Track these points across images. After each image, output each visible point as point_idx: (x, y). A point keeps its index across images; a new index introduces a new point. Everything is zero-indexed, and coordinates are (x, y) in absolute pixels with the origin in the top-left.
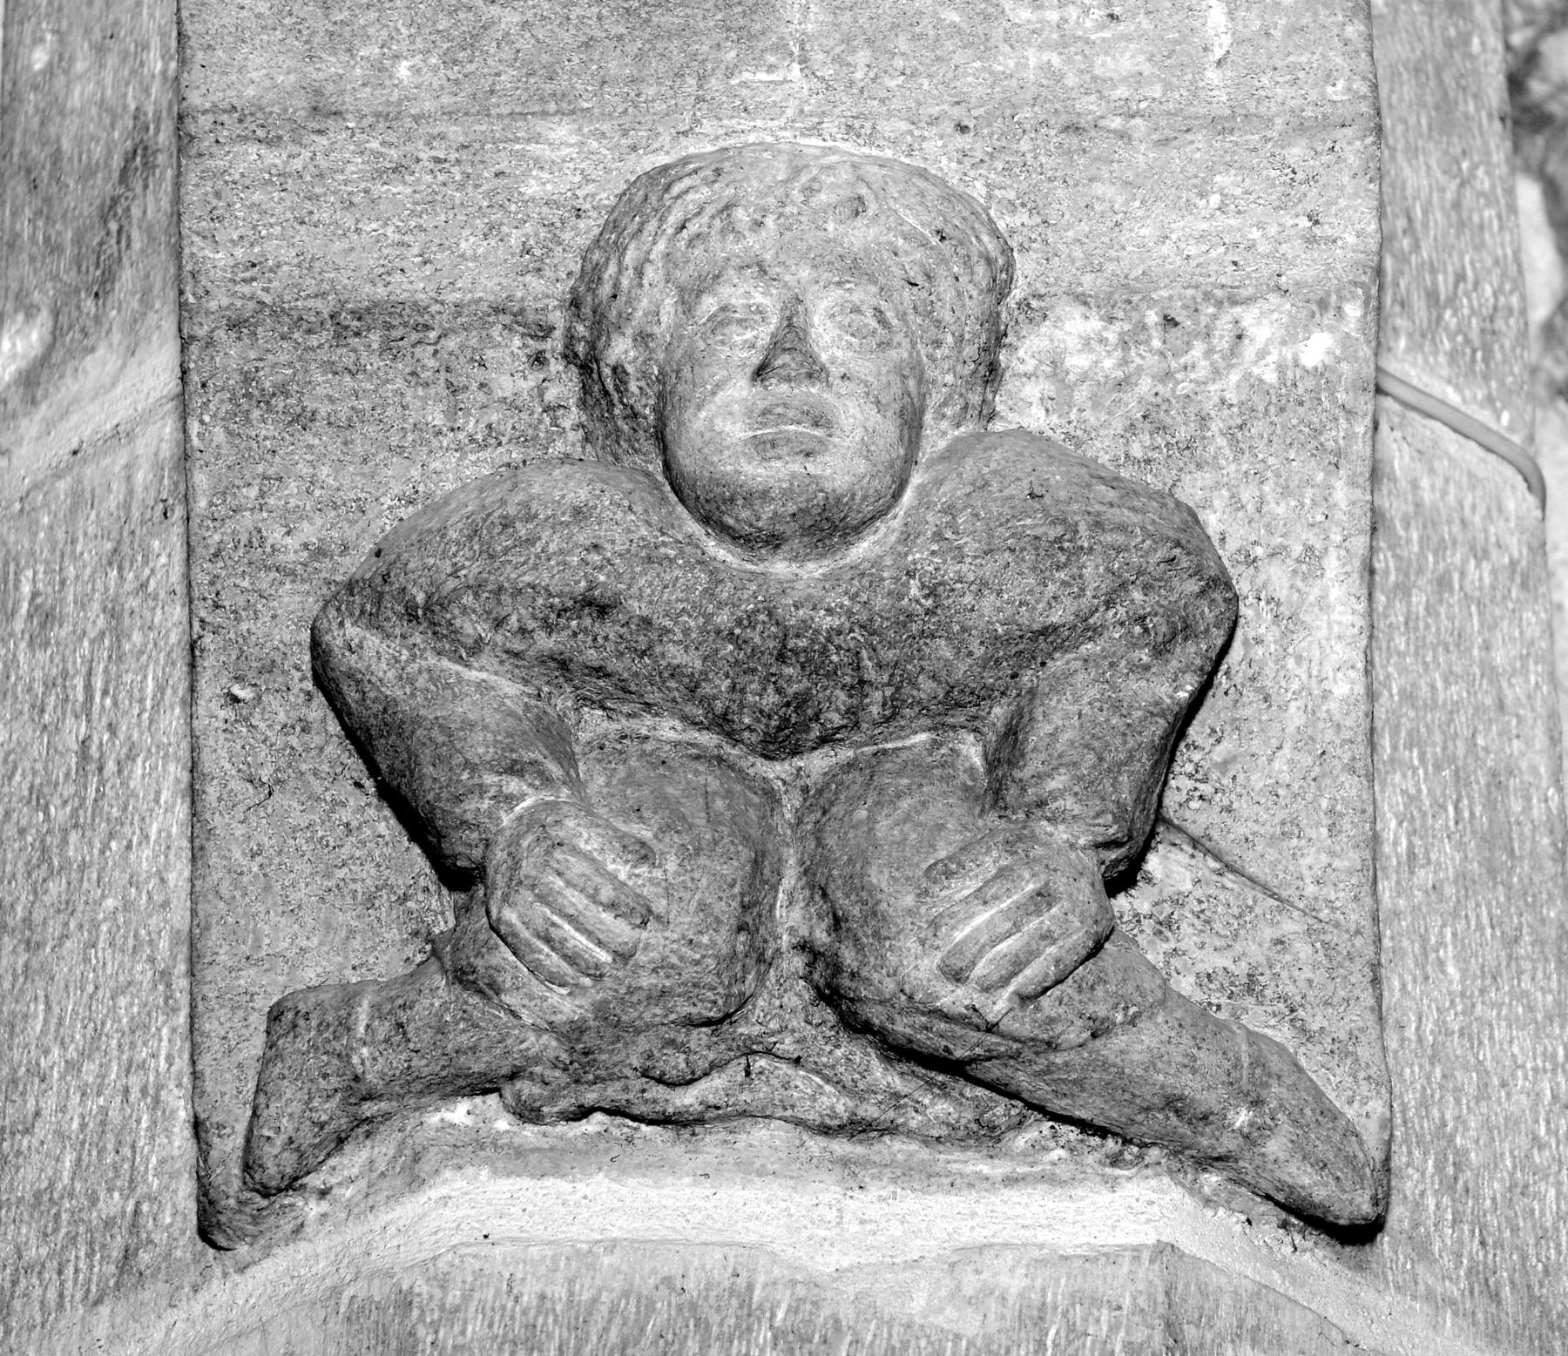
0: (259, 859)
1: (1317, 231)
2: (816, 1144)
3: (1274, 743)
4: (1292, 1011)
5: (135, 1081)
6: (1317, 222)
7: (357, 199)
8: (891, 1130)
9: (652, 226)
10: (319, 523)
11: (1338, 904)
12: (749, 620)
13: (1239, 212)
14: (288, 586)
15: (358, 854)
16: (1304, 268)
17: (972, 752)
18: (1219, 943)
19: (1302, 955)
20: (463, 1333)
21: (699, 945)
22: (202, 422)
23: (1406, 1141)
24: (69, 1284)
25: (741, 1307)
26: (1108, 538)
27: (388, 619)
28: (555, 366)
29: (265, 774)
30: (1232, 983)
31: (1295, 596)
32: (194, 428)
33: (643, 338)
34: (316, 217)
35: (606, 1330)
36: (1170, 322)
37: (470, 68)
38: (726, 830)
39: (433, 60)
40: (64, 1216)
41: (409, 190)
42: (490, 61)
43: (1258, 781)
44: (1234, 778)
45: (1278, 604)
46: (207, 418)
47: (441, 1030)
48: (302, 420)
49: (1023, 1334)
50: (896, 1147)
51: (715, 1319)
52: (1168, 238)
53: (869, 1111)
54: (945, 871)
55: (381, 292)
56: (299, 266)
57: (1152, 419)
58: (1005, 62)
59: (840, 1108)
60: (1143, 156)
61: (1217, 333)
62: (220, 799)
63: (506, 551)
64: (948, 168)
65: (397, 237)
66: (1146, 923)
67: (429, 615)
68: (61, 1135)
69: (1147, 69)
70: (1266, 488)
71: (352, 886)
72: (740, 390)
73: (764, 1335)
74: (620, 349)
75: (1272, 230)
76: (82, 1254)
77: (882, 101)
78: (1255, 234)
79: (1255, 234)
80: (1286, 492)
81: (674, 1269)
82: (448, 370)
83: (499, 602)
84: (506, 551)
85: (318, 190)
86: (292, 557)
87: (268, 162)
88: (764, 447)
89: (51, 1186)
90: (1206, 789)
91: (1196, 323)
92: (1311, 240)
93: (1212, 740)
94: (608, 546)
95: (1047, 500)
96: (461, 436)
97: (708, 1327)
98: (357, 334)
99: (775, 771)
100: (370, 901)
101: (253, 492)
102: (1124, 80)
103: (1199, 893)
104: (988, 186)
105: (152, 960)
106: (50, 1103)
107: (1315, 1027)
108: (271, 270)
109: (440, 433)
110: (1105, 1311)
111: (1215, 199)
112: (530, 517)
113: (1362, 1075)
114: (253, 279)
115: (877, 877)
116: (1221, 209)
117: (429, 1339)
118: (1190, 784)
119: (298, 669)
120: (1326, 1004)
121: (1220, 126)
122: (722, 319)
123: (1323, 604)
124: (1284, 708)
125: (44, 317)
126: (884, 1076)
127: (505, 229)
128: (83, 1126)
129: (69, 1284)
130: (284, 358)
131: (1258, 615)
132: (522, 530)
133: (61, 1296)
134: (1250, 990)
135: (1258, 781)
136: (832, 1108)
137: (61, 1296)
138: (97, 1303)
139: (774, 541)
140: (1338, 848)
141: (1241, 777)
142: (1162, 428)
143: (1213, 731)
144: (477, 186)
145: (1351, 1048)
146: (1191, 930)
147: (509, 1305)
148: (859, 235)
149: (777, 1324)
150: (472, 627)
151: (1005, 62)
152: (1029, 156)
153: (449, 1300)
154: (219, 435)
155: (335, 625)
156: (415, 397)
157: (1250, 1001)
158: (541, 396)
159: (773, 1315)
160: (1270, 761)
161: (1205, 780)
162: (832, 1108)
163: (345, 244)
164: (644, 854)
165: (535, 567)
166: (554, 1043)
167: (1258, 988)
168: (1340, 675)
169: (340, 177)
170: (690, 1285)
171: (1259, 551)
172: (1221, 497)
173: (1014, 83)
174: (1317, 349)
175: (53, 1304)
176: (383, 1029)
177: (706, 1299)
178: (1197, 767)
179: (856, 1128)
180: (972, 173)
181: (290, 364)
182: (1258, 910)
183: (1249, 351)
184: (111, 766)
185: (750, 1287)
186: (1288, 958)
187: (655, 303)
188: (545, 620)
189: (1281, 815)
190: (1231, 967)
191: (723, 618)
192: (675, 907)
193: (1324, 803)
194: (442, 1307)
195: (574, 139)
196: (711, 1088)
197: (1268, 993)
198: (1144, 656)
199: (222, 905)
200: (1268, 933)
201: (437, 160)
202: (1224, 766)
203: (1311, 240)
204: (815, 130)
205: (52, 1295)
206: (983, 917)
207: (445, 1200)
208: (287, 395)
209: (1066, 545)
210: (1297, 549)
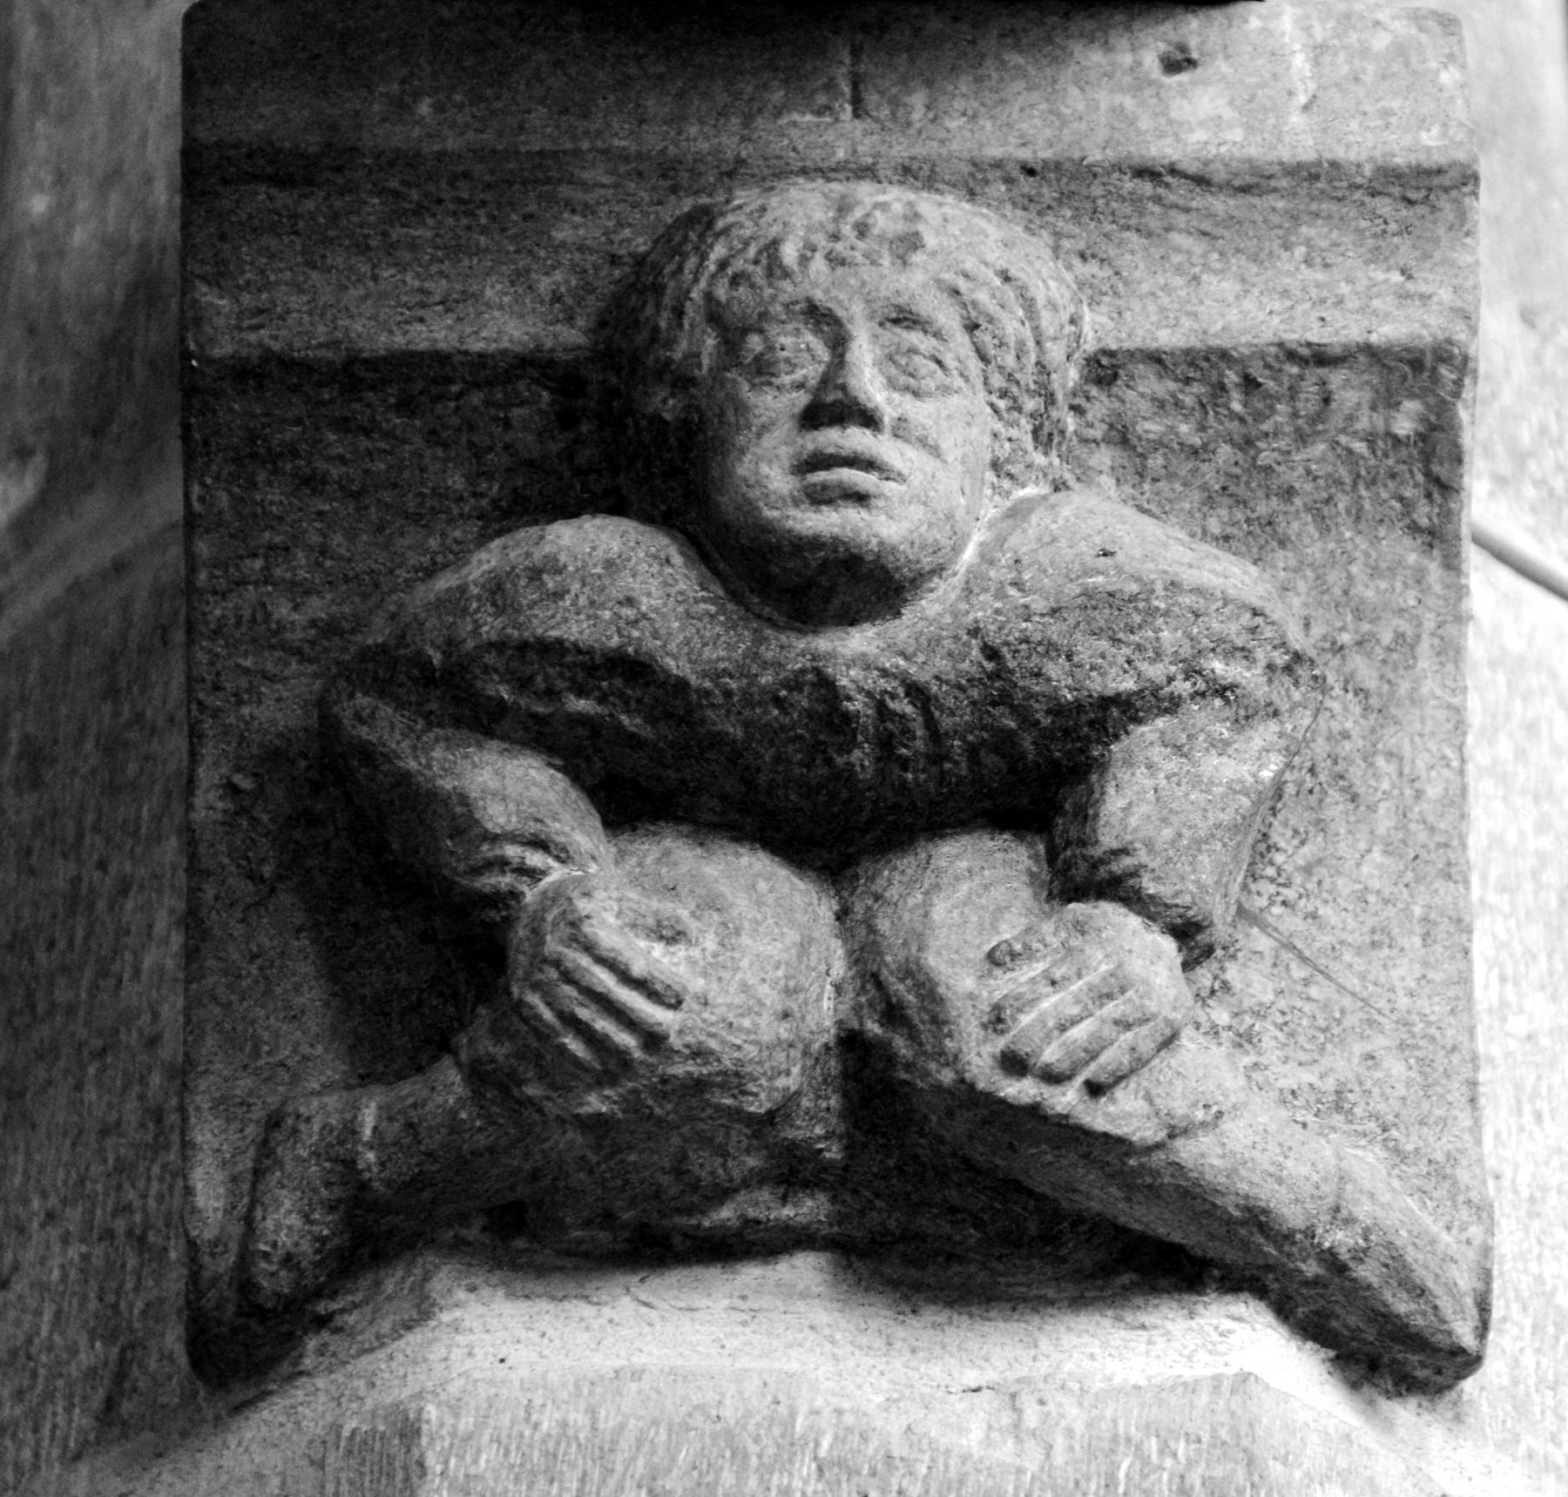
1: (1410, 286)
4: (1385, 1130)
6: (1410, 277)
7: (374, 243)
9: (692, 262)
11: (1433, 1018)
12: (794, 684)
15: (367, 955)
18: (1303, 1057)
19: (1394, 1071)
20: (475, 1462)
21: (740, 1029)
22: (203, 485)
23: (1503, 1294)
25: (783, 1436)
26: (1186, 600)
29: (267, 870)
30: (1319, 1101)
35: (634, 1459)
37: (499, 105)
40: (42, 1371)
41: (429, 234)
44: (1320, 883)
45: (1367, 695)
46: (209, 481)
48: (313, 483)
49: (1093, 1467)
51: (753, 1449)
56: (310, 313)
62: (217, 898)
65: (417, 283)
68: (41, 1287)
69: (1228, 114)
70: (1354, 569)
73: (807, 1467)
75: (1361, 285)
76: (60, 1410)
77: (942, 142)
78: (1344, 289)
79: (1344, 289)
81: (711, 1397)
82: (471, 428)
85: (332, 233)
86: (299, 635)
89: (29, 1341)
90: (1289, 894)
92: (1404, 296)
93: (1296, 842)
94: (644, 600)
97: (746, 1456)
98: (373, 388)
101: (258, 564)
102: (1201, 124)
103: (1282, 1004)
105: (141, 1097)
106: (30, 1255)
107: (1410, 1147)
109: (461, 498)
110: (1182, 1444)
111: (1300, 251)
114: (261, 326)
116: (1308, 261)
117: (439, 1468)
118: (1272, 889)
124: (1372, 808)
125: (39, 461)
128: (64, 1277)
129: (46, 1443)
131: (1345, 708)
132: (550, 582)
133: (37, 1455)
134: (1338, 1108)
135: (1345, 886)
136: (883, 1224)
137: (37, 1455)
138: (78, 1457)
141: (1326, 884)
143: (1296, 832)
144: (503, 230)
145: (1448, 1171)
146: (1273, 1043)
147: (527, 1433)
149: (822, 1453)
152: (1101, 202)
153: (462, 1427)
156: (435, 458)
158: (570, 458)
159: (817, 1445)
160: (1358, 865)
162: (883, 1224)
163: (361, 291)
166: (580, 1139)
167: (1347, 1106)
168: (1433, 774)
169: (354, 219)
170: (727, 1413)
171: (1345, 638)
177: (744, 1427)
178: (1279, 871)
181: (299, 422)
182: (1347, 1023)
184: (101, 905)
185: (793, 1414)
186: (1379, 1074)
189: (1371, 922)
192: (715, 986)
193: (1418, 911)
194: (453, 1434)
199: (217, 1010)
200: (1358, 1049)
201: (460, 201)
202: (1307, 870)
203: (1404, 296)
205: (27, 1454)
208: (295, 454)
210: (1387, 637)
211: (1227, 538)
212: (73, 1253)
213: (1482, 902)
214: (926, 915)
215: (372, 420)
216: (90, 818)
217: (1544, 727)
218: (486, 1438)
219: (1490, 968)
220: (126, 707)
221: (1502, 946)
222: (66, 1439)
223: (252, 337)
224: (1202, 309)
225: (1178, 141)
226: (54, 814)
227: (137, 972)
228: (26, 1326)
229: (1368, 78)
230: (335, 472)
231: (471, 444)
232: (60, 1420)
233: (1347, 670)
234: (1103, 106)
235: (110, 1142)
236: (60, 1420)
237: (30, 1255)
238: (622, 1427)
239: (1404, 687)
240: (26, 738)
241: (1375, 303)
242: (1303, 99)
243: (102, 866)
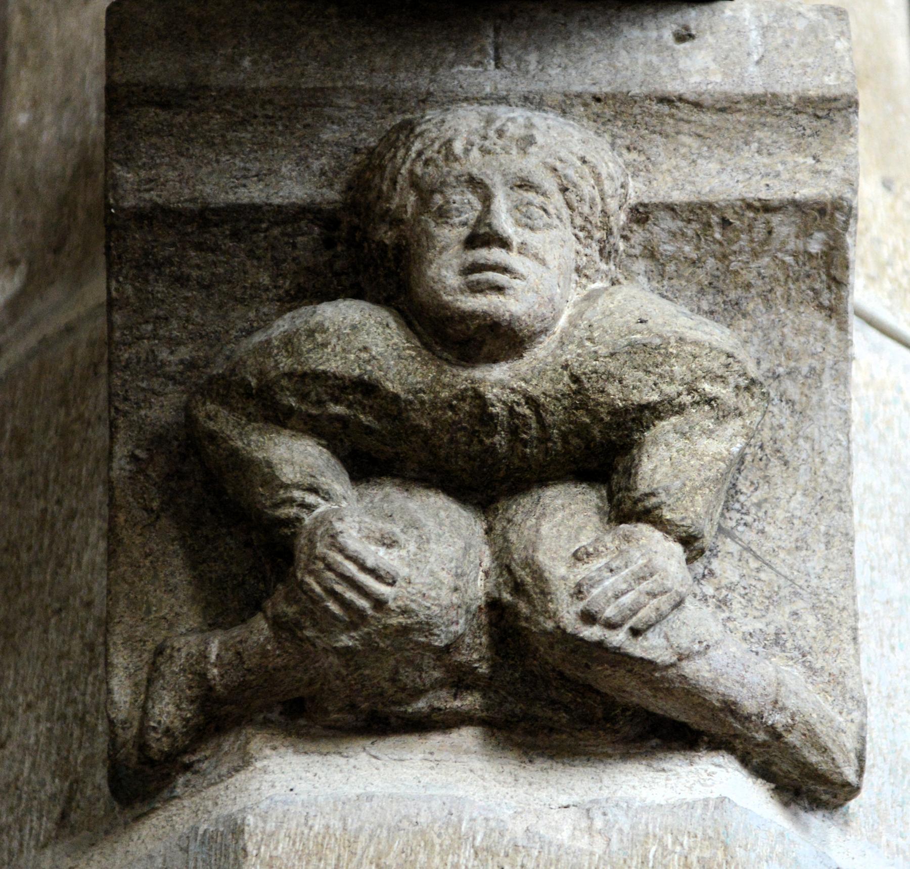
0: (150, 558)
3: (791, 491)
4: (804, 656)
5: (70, 711)
6: (818, 161)
7: (217, 141)
9: (401, 153)
10: (191, 346)
11: (831, 591)
13: (770, 154)
14: (171, 387)
15: (213, 555)
18: (757, 614)
19: (809, 622)
20: (276, 848)
21: (429, 597)
22: (118, 281)
24: (27, 837)
25: (454, 833)
26: (688, 348)
27: (233, 397)
30: (765, 639)
31: (804, 398)
32: (114, 284)
34: (191, 152)
37: (290, 61)
38: (446, 529)
39: (265, 57)
40: (24, 796)
41: (249, 136)
42: (301, 57)
44: (766, 512)
46: (121, 279)
51: (437, 841)
55: (232, 197)
56: (180, 182)
59: (517, 711)
61: (756, 230)
62: (126, 521)
63: (309, 351)
65: (242, 165)
66: (710, 600)
69: (713, 66)
70: (785, 330)
71: (209, 575)
75: (790, 166)
76: (35, 818)
77: (547, 82)
78: (780, 167)
79: (780, 167)
80: (797, 332)
83: (304, 384)
84: (309, 351)
85: (192, 135)
86: (173, 368)
87: (161, 118)
89: (17, 779)
90: (749, 519)
91: (743, 223)
93: (752, 489)
95: (650, 323)
96: (281, 292)
97: (433, 845)
98: (216, 225)
101: (150, 327)
103: (743, 583)
104: (613, 136)
106: (17, 729)
107: (818, 666)
108: (163, 184)
110: (686, 838)
111: (755, 146)
112: (325, 331)
113: (848, 696)
114: (152, 189)
117: (255, 852)
118: (738, 516)
119: (177, 439)
120: (825, 652)
124: (796, 469)
127: (310, 160)
128: (37, 741)
129: (27, 837)
130: (168, 240)
131: (781, 411)
132: (319, 338)
133: (21, 845)
134: (777, 643)
135: (780, 514)
136: (513, 711)
137: (21, 845)
138: (45, 846)
140: (831, 557)
141: (770, 512)
142: (721, 292)
143: (752, 483)
146: (739, 606)
152: (639, 117)
154: (129, 290)
155: (200, 404)
157: (776, 650)
159: (474, 839)
160: (788, 502)
161: (747, 514)
162: (513, 711)
163: (210, 169)
165: (328, 360)
167: (782, 642)
169: (206, 127)
171: (781, 370)
172: (757, 335)
173: (629, 73)
175: (16, 850)
180: (602, 128)
181: (173, 245)
182: (781, 594)
184: (59, 525)
185: (460, 821)
186: (800, 623)
188: (332, 395)
189: (795, 536)
190: (765, 629)
193: (823, 528)
194: (263, 832)
195: (353, 104)
197: (788, 645)
199: (126, 586)
201: (267, 117)
202: (759, 505)
205: (15, 844)
209: (662, 351)
211: (712, 313)
212: (43, 727)
218: (282, 835)
222: (38, 834)
223: (147, 196)
224: (697, 179)
228: (15, 770)
235: (63, 663)
238: (361, 829)
241: (798, 176)
243: (59, 502)
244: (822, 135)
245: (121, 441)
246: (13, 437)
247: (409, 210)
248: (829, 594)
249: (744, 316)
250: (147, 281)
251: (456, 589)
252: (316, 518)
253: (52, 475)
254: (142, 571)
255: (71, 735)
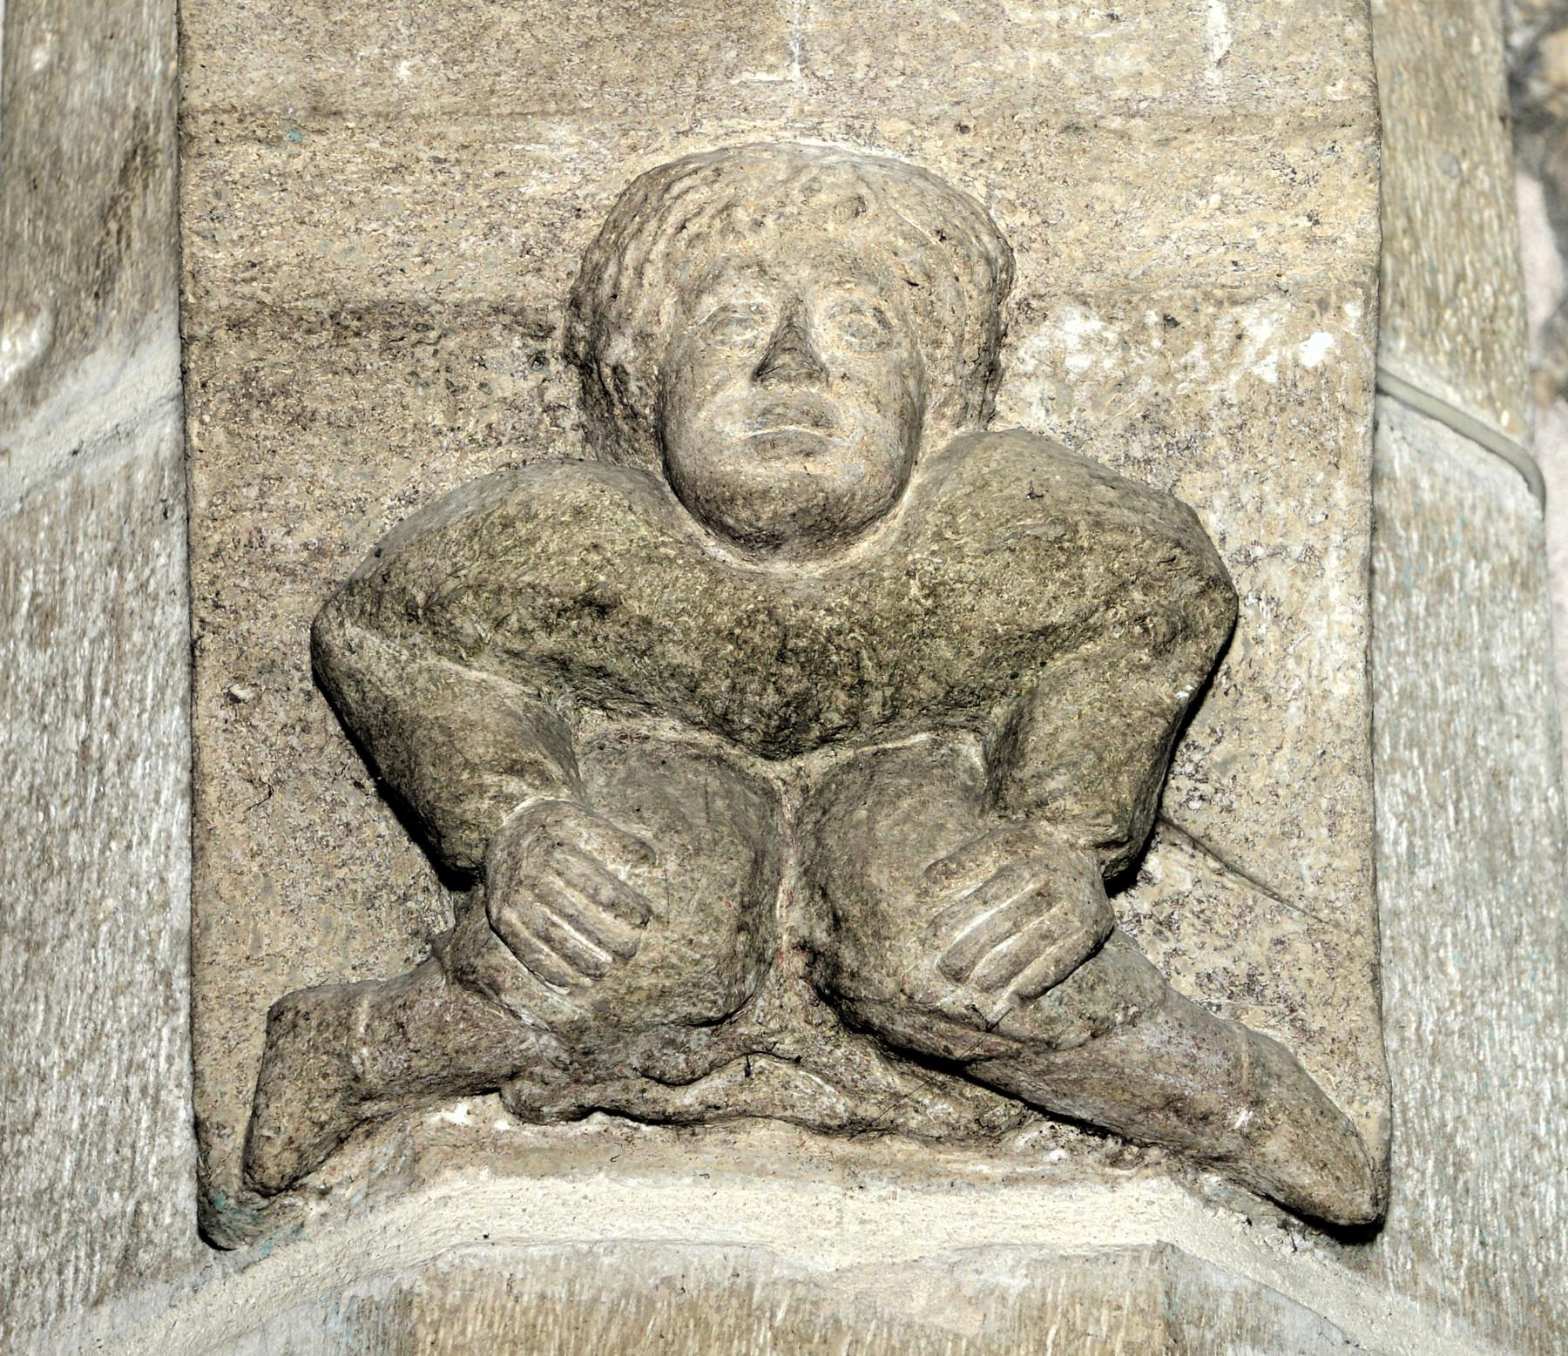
0: (259, 859)
1: (1317, 230)
2: (816, 1144)
3: (1275, 743)
6: (1317, 222)
7: (356, 200)
8: (891, 1129)
9: (652, 226)
12: (750, 620)
16: (1303, 269)
17: (972, 752)
18: (1219, 943)
19: (1302, 955)
20: (463, 1332)
21: (700, 945)
22: (202, 422)
24: (70, 1284)
27: (388, 619)
28: (555, 366)
32: (195, 427)
33: (643, 338)
35: (606, 1329)
36: (1169, 322)
37: (470, 68)
38: (726, 830)
40: (65, 1217)
43: (1258, 781)
46: (207, 418)
47: (441, 1029)
48: (302, 420)
50: (897, 1147)
51: (715, 1318)
52: (1167, 238)
53: (869, 1110)
54: (944, 871)
56: (299, 266)
57: (1152, 418)
58: (1006, 62)
59: (840, 1108)
60: (1143, 155)
62: (220, 799)
63: (506, 551)
64: (948, 168)
66: (1146, 923)
67: (429, 616)
68: (63, 1136)
69: (1147, 69)
70: (1266, 488)
71: (352, 886)
72: (740, 389)
73: (764, 1335)
74: (621, 349)
77: (883, 101)
78: (1255, 234)
79: (1255, 234)
83: (499, 602)
84: (506, 551)
85: (318, 190)
86: (292, 557)
87: (268, 161)
88: (763, 447)
89: (51, 1187)
90: (1205, 789)
92: (1311, 241)
94: (609, 546)
95: (1048, 500)
97: (708, 1327)
98: (357, 334)
99: (776, 771)
100: (370, 901)
101: (253, 492)
102: (1125, 79)
103: (1199, 893)
105: (152, 960)
106: (51, 1103)
107: (1315, 1027)
109: (440, 433)
110: (1105, 1311)
111: (1215, 199)
113: (1362, 1074)
114: (253, 279)
115: (877, 876)
117: (429, 1339)
118: (1190, 784)
121: (1221, 126)
122: (721, 320)
123: (1323, 604)
124: (1284, 708)
126: (885, 1076)
127: (505, 229)
128: (83, 1127)
129: (70, 1284)
132: (523, 530)
133: (61, 1296)
134: (1250, 990)
135: (1258, 781)
136: (832, 1108)
137: (61, 1296)
138: (98, 1302)
139: (774, 541)
141: (1241, 777)
143: (1213, 731)
144: (477, 186)
148: (860, 236)
150: (472, 627)
151: (1006, 62)
153: (449, 1300)
154: (219, 435)
155: (335, 625)
158: (541, 396)
159: (773, 1315)
160: (1270, 761)
161: (1205, 780)
162: (832, 1108)
163: (345, 244)
164: (644, 854)
169: (339, 177)
170: (690, 1285)
171: (1259, 552)
174: (1317, 349)
176: (383, 1029)
177: (706, 1299)
178: (1197, 767)
179: (856, 1128)
182: (1258, 910)
183: (1249, 351)
184: (111, 767)
185: (750, 1287)
186: (1288, 957)
187: (655, 303)
188: (545, 620)
191: (723, 618)
193: (1324, 804)
194: (442, 1308)
195: (574, 139)
196: (711, 1088)
197: (1269, 993)
198: (1144, 656)
200: (1268, 934)
201: (437, 160)
202: (1224, 766)
204: (816, 130)
205: (52, 1294)
206: (982, 917)
207: (445, 1200)
211: (1148, 461)
212: (94, 1104)
213: (1392, 760)
214: (871, 829)
215: (357, 362)
216: (98, 683)
217: (1456, 577)
218: (472, 1309)
219: (1400, 824)
220: (130, 576)
221: (1413, 799)
222: (88, 1282)
223: (246, 289)
224: (1123, 254)
225: (1102, 98)
226: (65, 675)
227: (145, 837)
228: (50, 1172)
229: (1276, 34)
230: (325, 408)
231: (449, 384)
232: (83, 1266)
233: (1259, 581)
234: (1033, 62)
235: (122, 1001)
236: (83, 1266)
237: (51, 1103)
238: (595, 1300)
239: (1314, 594)
240: (35, 594)
241: (1284, 248)
242: (1218, 53)
243: (112, 728)
244: (1323, 180)
245: (210, 672)
246: (35, 609)
247: (664, 318)
248: (1334, 910)
249: (1199, 466)
250: (247, 419)
251: (741, 928)
252: (520, 818)
253: (98, 683)
254: (245, 879)
255: (138, 1122)
